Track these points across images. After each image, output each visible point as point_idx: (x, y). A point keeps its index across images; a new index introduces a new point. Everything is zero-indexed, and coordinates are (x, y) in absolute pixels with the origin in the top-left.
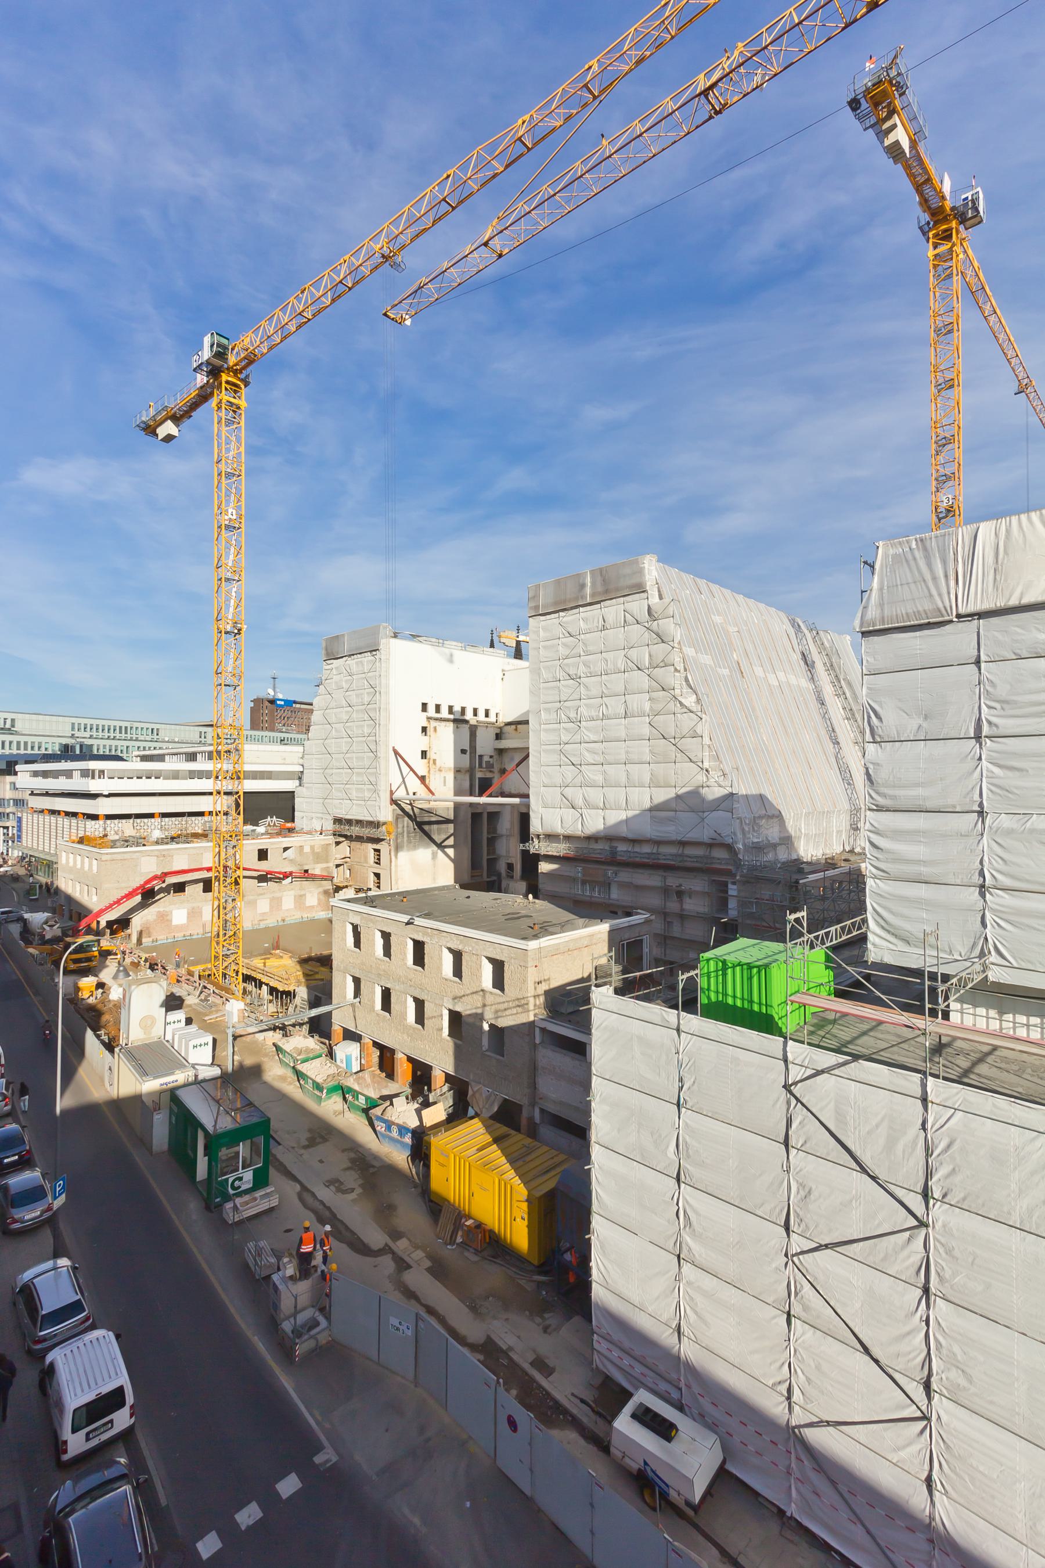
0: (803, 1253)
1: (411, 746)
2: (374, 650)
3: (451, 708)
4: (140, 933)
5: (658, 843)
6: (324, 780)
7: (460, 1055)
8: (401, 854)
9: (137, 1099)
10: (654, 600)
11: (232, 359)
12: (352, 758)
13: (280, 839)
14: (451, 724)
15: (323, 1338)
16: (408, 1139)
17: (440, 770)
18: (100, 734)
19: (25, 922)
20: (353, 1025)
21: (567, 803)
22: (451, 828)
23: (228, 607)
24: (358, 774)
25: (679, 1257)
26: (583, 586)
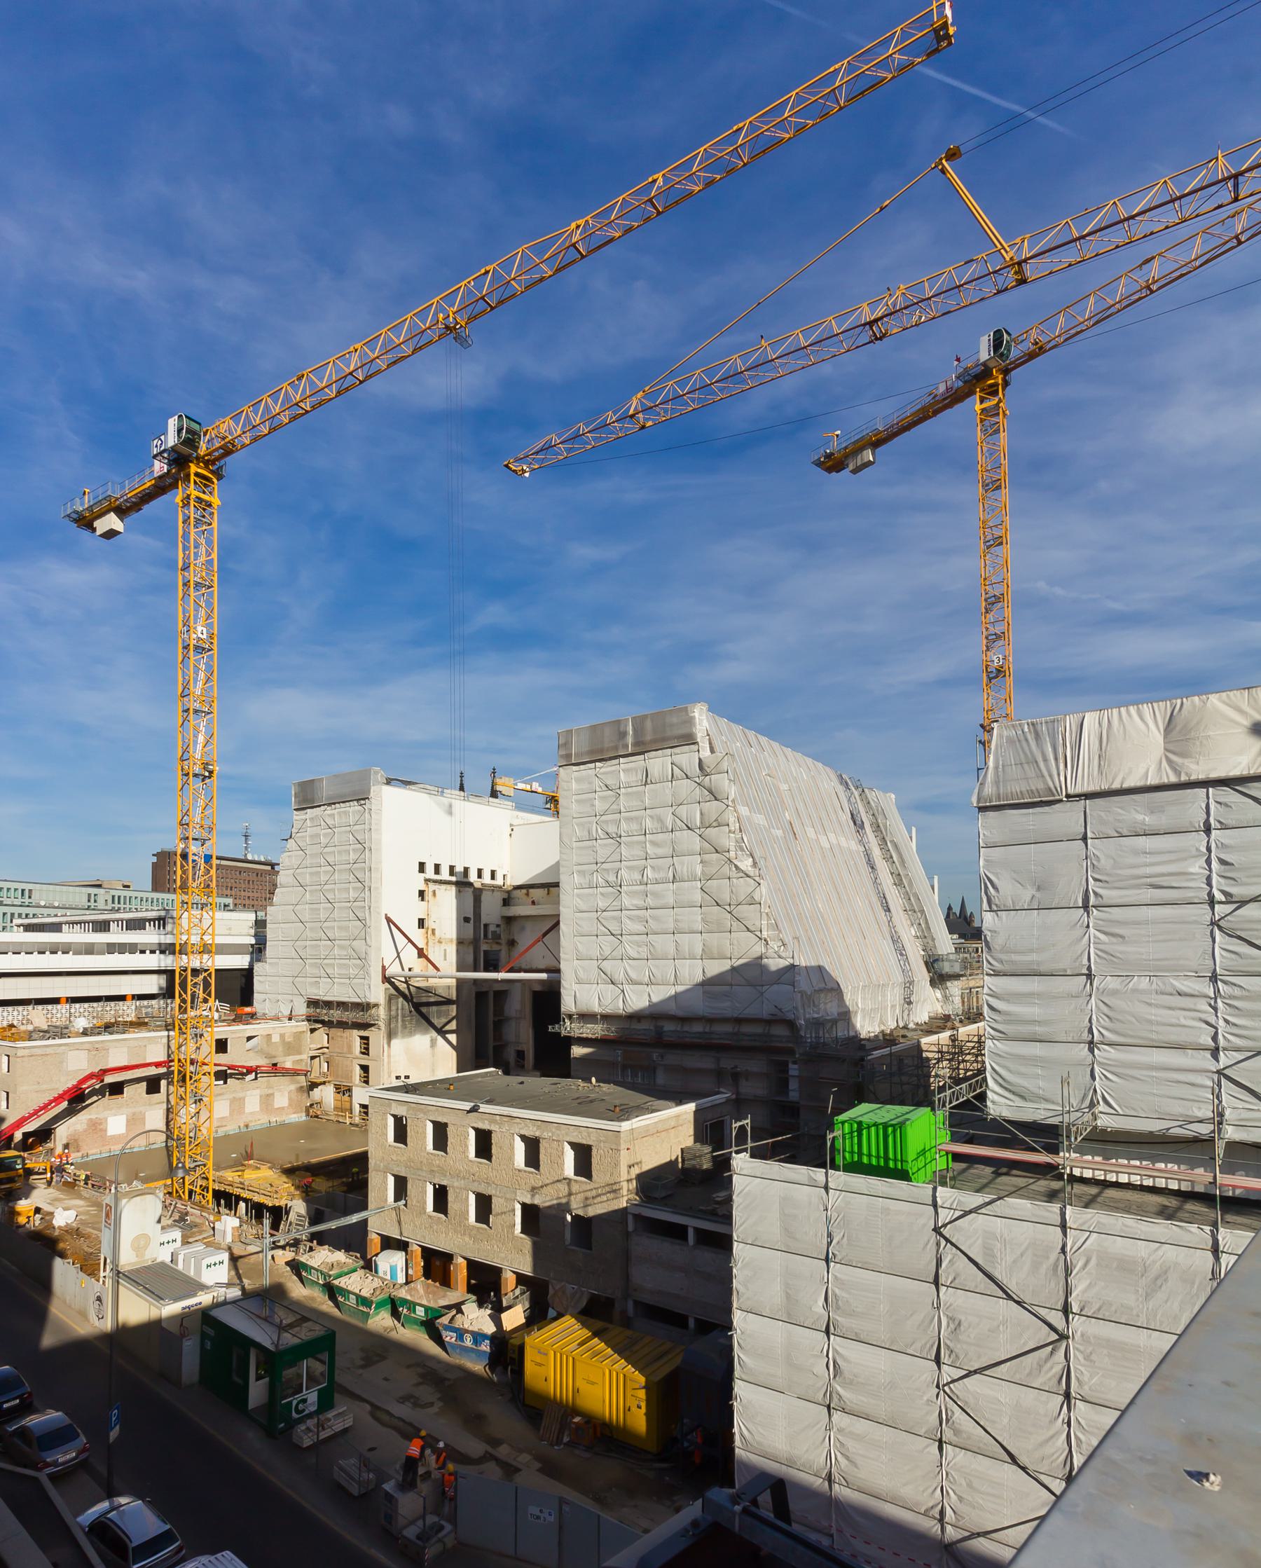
0: (953, 1381)
1: (407, 912)
3: (452, 868)
5: (710, 1020)
6: (294, 954)
7: (538, 1254)
8: (394, 1042)
9: (153, 1328)
10: (705, 753)
11: (203, 449)
12: (333, 928)
13: (241, 1027)
14: (454, 888)
15: (450, 1542)
16: (485, 1347)
17: (440, 942)
20: (397, 1231)
21: (605, 975)
22: (453, 1010)
24: (341, 947)
25: (829, 1407)
26: (623, 735)
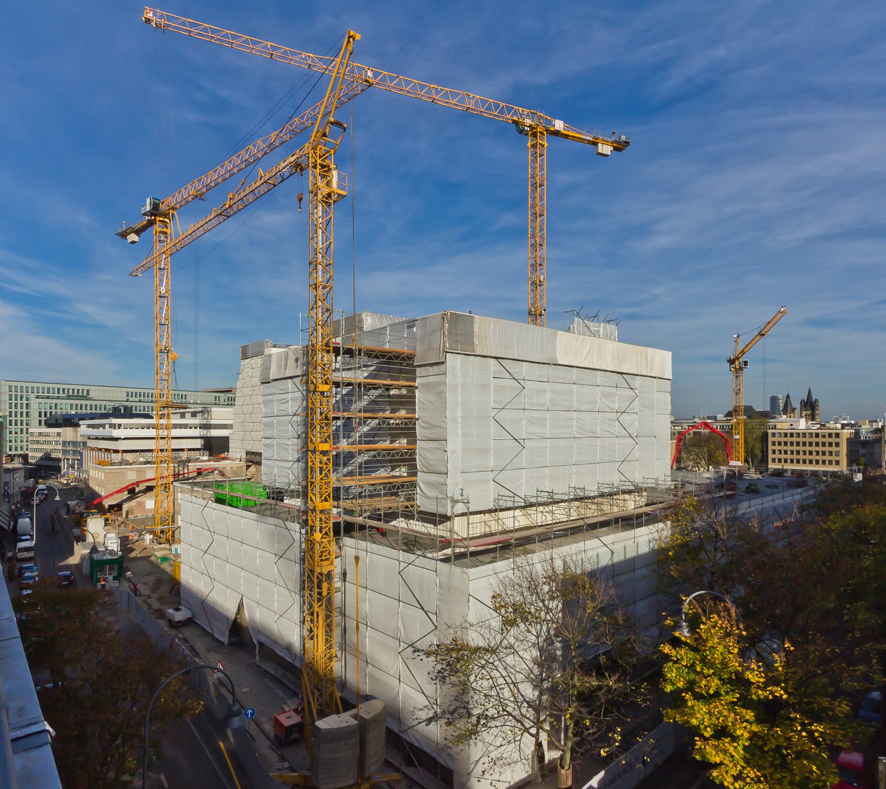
4: (127, 513)
18: (146, 399)
19: (68, 505)
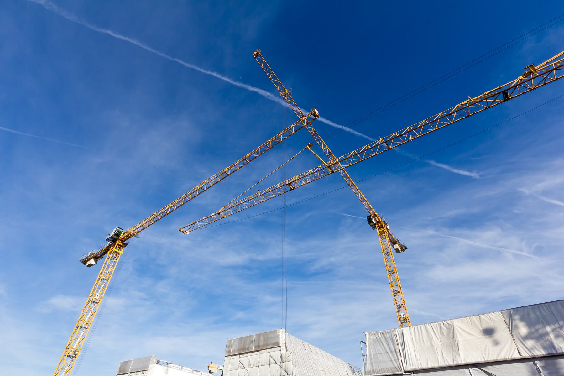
2: (144, 370)
10: (284, 351)
11: (122, 236)
23: (74, 344)
